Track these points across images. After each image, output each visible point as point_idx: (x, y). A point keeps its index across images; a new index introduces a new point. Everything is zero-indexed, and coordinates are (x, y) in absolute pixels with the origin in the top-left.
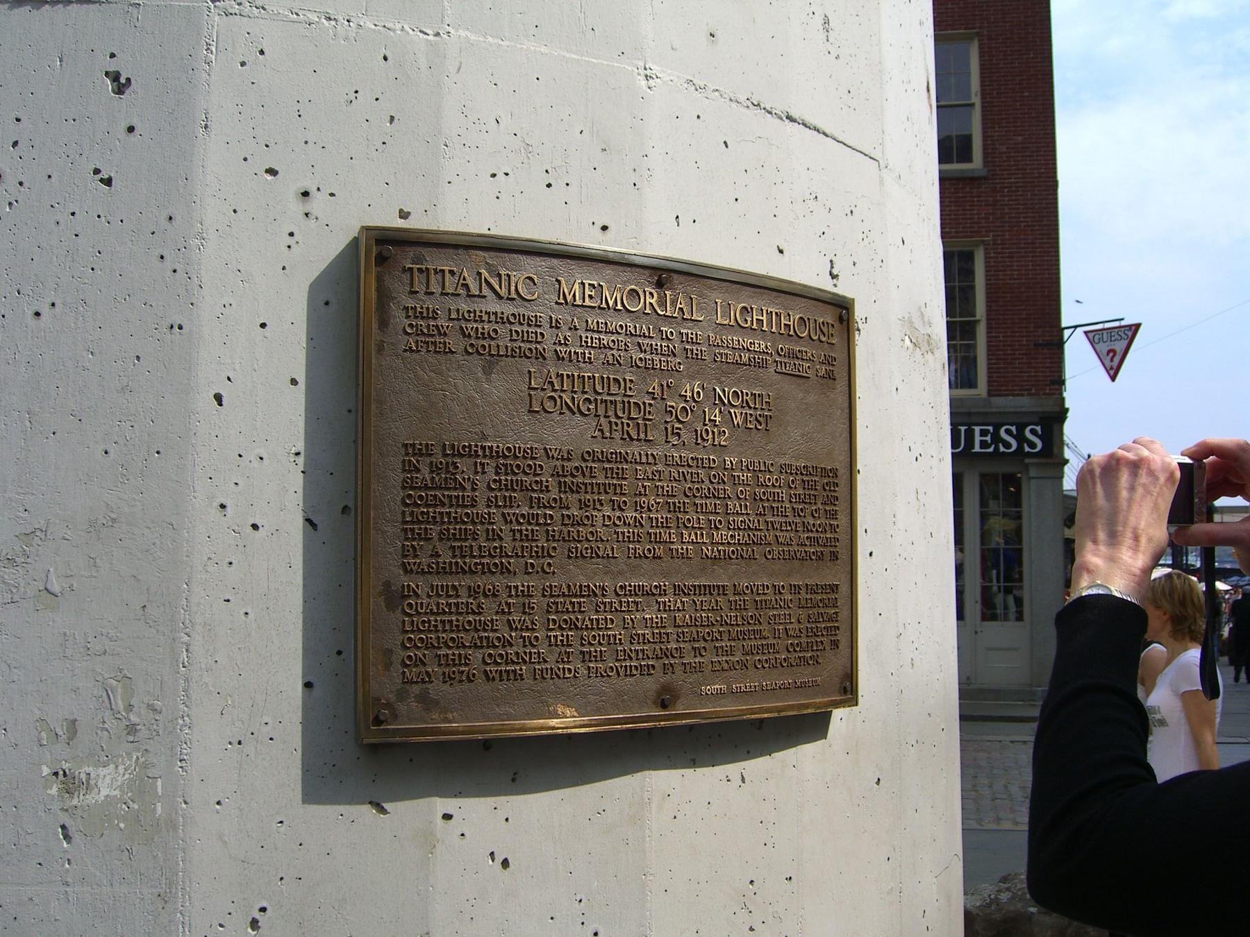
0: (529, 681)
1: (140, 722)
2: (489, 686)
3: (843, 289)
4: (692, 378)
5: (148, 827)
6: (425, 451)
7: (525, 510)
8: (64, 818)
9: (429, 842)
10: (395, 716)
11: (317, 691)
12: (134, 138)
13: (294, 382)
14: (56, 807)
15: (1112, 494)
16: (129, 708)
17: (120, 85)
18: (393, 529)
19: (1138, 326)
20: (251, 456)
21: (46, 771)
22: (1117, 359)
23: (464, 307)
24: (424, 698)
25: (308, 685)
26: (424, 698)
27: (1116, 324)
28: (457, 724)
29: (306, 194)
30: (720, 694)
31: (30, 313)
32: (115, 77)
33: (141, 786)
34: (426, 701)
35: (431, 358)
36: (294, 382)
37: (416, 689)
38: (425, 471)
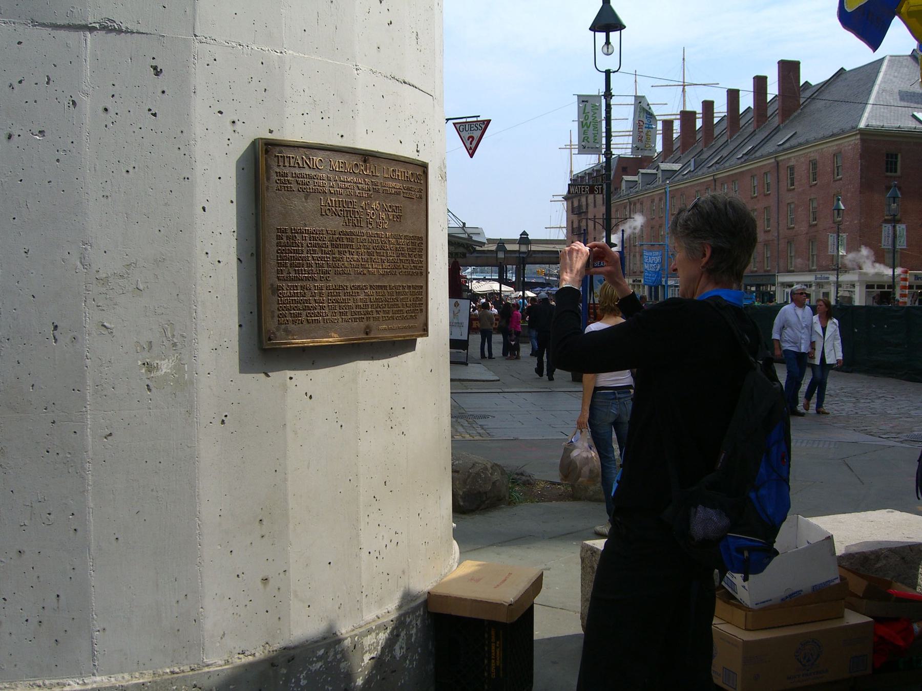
0: (322, 323)
1: (177, 341)
2: (308, 325)
3: (422, 158)
4: (375, 200)
5: (182, 384)
6: (285, 231)
7: (320, 255)
8: (148, 382)
9: (285, 388)
10: (276, 338)
11: (244, 328)
12: (165, 96)
13: (232, 202)
14: (144, 378)
15: (571, 259)
16: (173, 336)
17: (157, 72)
18: (273, 263)
19: (489, 121)
20: (216, 232)
21: (140, 363)
22: (474, 143)
23: (297, 172)
24: (286, 330)
25: (240, 326)
26: (286, 330)
27: (475, 119)
28: (298, 341)
29: (234, 122)
30: (385, 329)
31: (124, 171)
32: (155, 68)
33: (179, 367)
34: (287, 332)
35: (286, 193)
36: (232, 202)
37: (283, 326)
38: (285, 239)
